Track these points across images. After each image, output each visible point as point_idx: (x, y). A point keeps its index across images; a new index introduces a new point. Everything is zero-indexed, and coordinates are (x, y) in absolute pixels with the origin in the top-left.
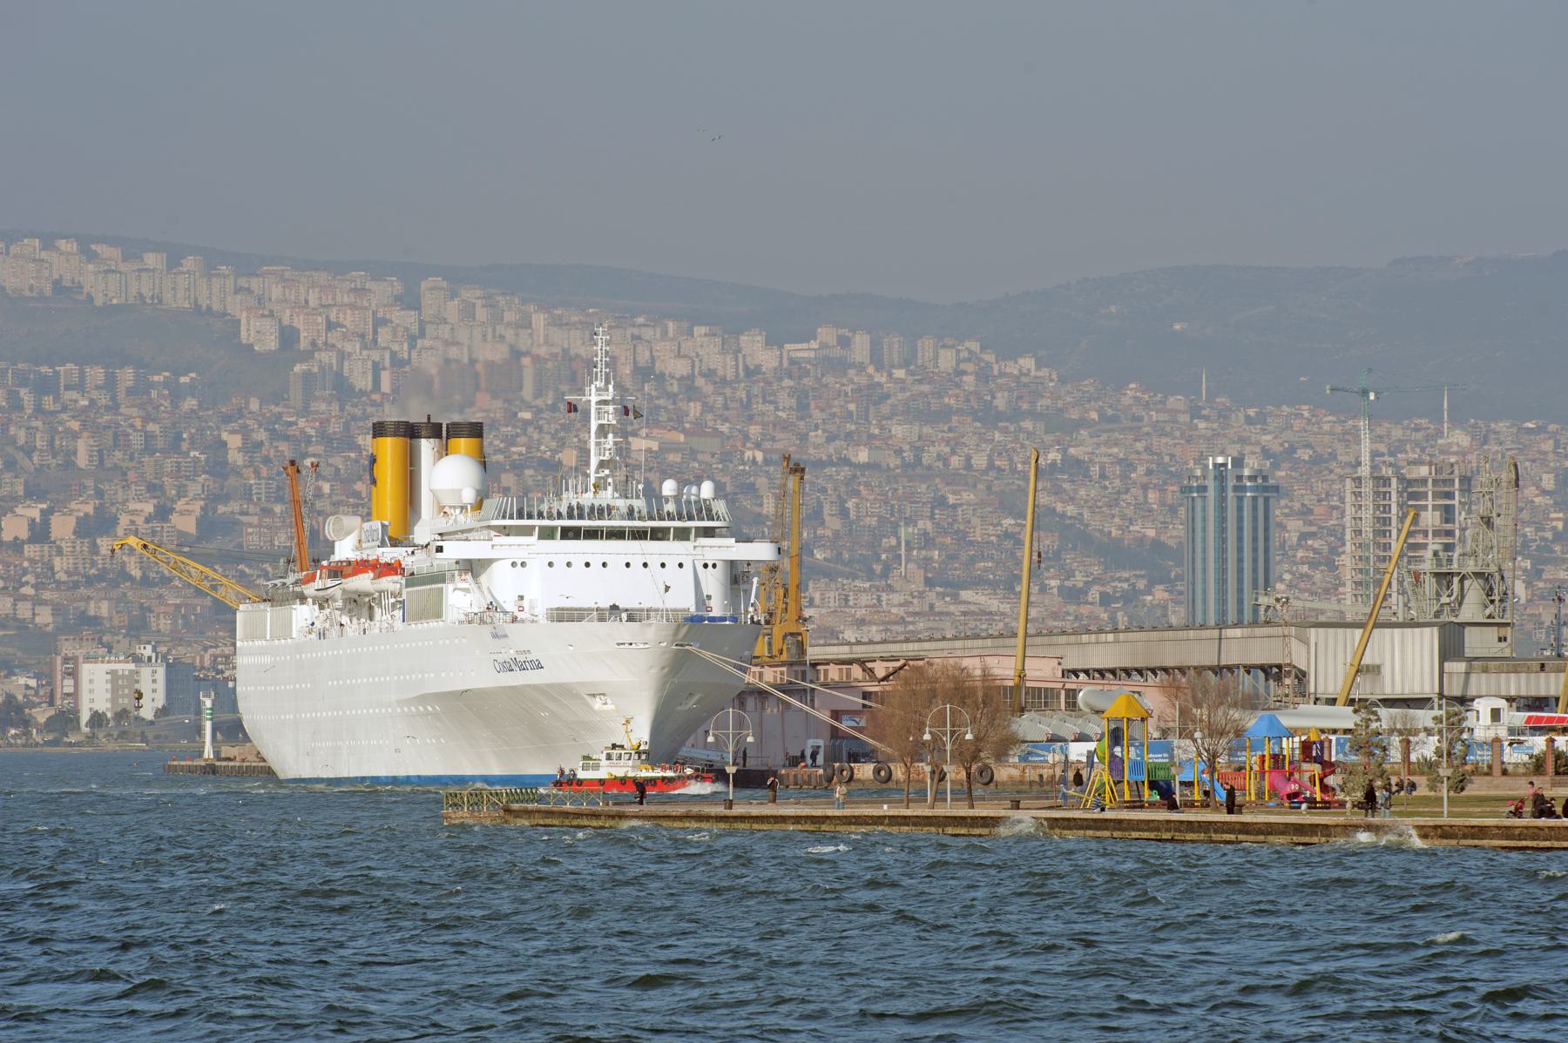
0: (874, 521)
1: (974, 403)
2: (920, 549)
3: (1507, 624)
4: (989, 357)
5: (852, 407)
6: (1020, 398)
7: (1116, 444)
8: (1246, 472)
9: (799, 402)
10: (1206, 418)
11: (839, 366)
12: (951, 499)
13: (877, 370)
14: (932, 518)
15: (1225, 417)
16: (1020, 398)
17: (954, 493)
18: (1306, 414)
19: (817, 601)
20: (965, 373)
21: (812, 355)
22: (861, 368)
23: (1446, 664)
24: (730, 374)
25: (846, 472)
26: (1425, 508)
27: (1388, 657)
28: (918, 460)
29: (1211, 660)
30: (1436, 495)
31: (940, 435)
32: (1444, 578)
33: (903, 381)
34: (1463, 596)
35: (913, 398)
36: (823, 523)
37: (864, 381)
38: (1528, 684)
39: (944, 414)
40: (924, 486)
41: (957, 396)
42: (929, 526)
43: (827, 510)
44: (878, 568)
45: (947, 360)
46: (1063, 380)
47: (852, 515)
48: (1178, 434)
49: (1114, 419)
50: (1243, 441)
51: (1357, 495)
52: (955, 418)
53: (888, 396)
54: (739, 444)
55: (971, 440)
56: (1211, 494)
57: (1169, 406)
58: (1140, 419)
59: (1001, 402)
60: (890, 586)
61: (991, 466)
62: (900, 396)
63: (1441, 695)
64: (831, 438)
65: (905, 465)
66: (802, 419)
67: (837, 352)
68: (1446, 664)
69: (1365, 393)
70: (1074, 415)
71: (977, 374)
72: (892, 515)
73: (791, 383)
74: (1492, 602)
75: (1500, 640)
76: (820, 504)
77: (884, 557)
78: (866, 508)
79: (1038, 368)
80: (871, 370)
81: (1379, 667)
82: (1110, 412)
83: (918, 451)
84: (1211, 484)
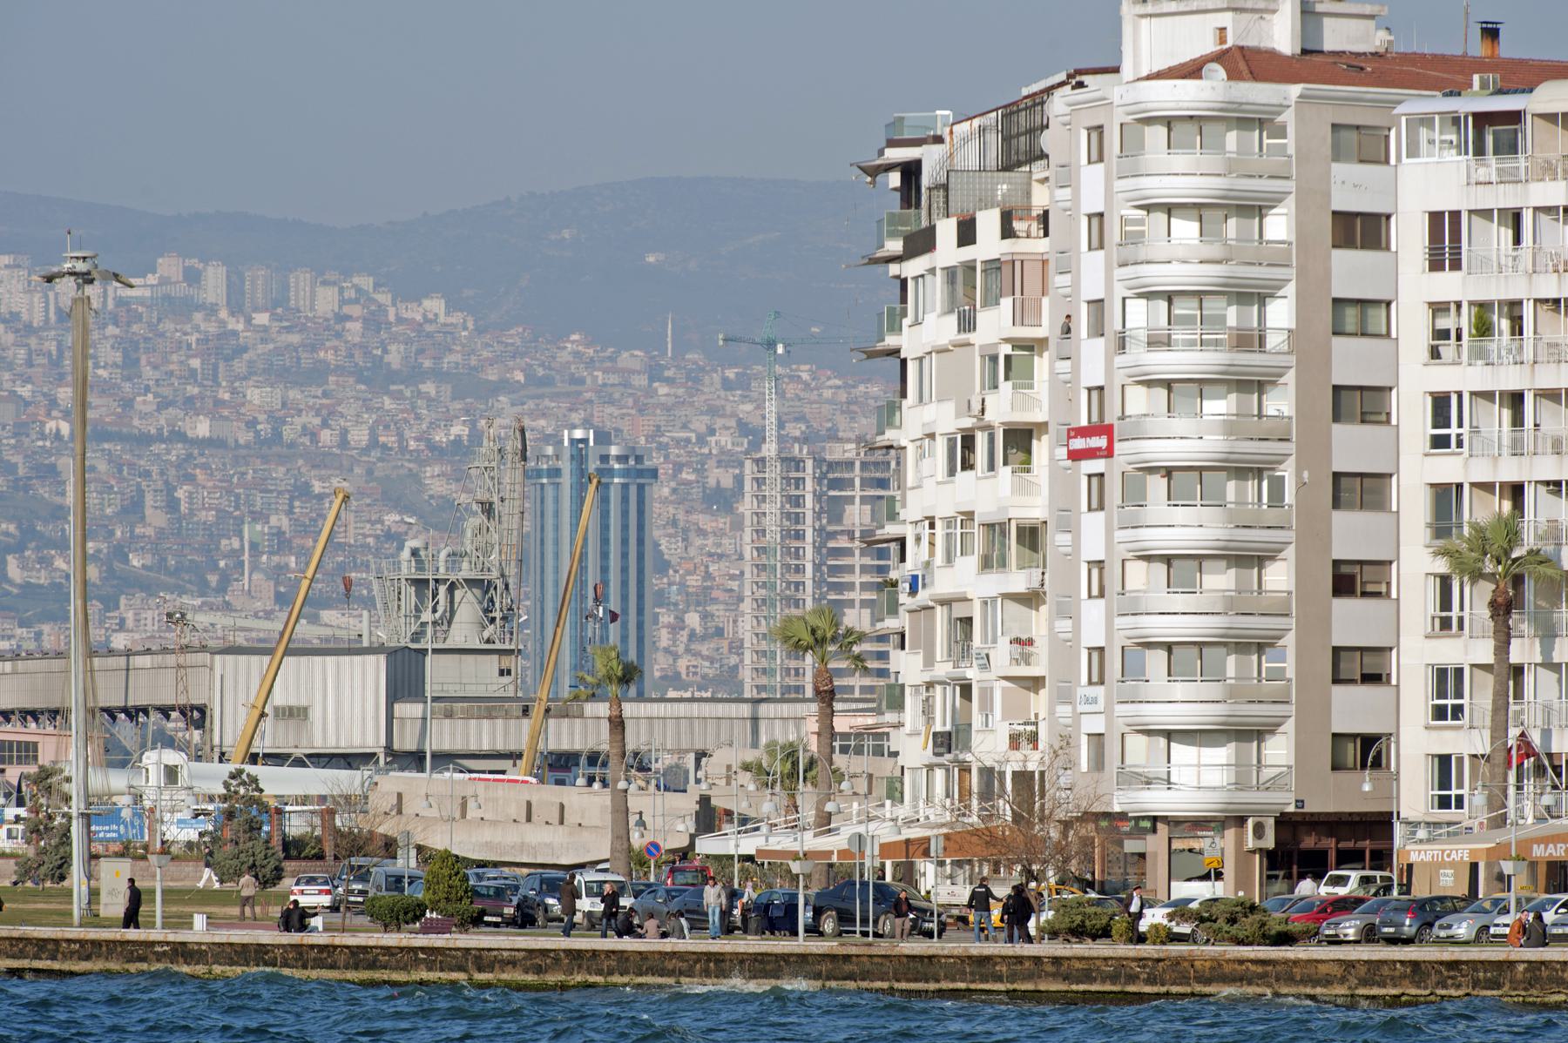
0: (211, 516)
1: (359, 359)
2: (271, 553)
3: (510, 652)
4: (384, 298)
5: (195, 363)
6: (421, 352)
7: (544, 415)
8: (614, 451)
9: (126, 356)
10: (670, 381)
11: (181, 308)
12: (317, 487)
13: (232, 314)
14: (290, 511)
15: (697, 380)
16: (421, 352)
17: (322, 479)
18: (805, 376)
19: (130, 623)
20: (348, 318)
21: (148, 293)
22: (212, 310)
23: (397, 706)
24: (37, 321)
25: (178, 450)
26: (851, 500)
27: (318, 697)
28: (277, 435)
29: (118, 702)
30: (865, 483)
31: (311, 402)
32: (420, 584)
33: (265, 329)
34: (453, 612)
35: (278, 352)
36: (143, 518)
37: (212, 328)
38: (506, 734)
39: (318, 374)
40: (282, 469)
41: (336, 349)
42: (285, 523)
43: (149, 500)
44: (213, 579)
45: (327, 301)
46: (480, 331)
47: (184, 507)
48: (630, 401)
49: (546, 381)
50: (714, 411)
51: (760, 482)
52: (332, 379)
53: (245, 349)
54: (42, 411)
55: (349, 409)
56: (566, 480)
57: (620, 365)
58: (582, 381)
59: (395, 357)
60: (228, 604)
61: (374, 443)
62: (261, 348)
63: (389, 749)
64: (163, 405)
65: (260, 442)
66: (129, 379)
67: (181, 290)
68: (397, 706)
69: (771, 345)
70: (492, 375)
71: (365, 320)
72: (237, 508)
73: (117, 331)
74: (493, 620)
75: (502, 673)
76: (141, 493)
77: (222, 564)
78: (201, 499)
79: (447, 314)
80: (223, 314)
81: (306, 709)
82: (541, 372)
83: (277, 422)
84: (566, 466)
